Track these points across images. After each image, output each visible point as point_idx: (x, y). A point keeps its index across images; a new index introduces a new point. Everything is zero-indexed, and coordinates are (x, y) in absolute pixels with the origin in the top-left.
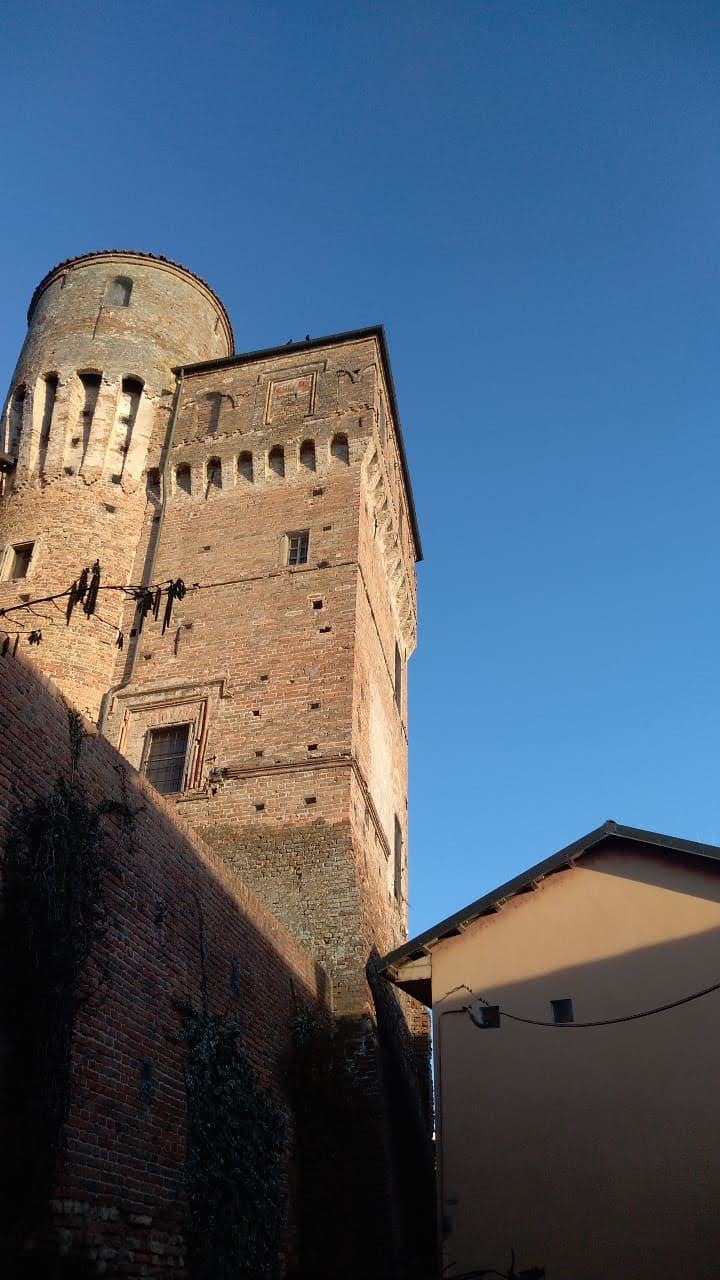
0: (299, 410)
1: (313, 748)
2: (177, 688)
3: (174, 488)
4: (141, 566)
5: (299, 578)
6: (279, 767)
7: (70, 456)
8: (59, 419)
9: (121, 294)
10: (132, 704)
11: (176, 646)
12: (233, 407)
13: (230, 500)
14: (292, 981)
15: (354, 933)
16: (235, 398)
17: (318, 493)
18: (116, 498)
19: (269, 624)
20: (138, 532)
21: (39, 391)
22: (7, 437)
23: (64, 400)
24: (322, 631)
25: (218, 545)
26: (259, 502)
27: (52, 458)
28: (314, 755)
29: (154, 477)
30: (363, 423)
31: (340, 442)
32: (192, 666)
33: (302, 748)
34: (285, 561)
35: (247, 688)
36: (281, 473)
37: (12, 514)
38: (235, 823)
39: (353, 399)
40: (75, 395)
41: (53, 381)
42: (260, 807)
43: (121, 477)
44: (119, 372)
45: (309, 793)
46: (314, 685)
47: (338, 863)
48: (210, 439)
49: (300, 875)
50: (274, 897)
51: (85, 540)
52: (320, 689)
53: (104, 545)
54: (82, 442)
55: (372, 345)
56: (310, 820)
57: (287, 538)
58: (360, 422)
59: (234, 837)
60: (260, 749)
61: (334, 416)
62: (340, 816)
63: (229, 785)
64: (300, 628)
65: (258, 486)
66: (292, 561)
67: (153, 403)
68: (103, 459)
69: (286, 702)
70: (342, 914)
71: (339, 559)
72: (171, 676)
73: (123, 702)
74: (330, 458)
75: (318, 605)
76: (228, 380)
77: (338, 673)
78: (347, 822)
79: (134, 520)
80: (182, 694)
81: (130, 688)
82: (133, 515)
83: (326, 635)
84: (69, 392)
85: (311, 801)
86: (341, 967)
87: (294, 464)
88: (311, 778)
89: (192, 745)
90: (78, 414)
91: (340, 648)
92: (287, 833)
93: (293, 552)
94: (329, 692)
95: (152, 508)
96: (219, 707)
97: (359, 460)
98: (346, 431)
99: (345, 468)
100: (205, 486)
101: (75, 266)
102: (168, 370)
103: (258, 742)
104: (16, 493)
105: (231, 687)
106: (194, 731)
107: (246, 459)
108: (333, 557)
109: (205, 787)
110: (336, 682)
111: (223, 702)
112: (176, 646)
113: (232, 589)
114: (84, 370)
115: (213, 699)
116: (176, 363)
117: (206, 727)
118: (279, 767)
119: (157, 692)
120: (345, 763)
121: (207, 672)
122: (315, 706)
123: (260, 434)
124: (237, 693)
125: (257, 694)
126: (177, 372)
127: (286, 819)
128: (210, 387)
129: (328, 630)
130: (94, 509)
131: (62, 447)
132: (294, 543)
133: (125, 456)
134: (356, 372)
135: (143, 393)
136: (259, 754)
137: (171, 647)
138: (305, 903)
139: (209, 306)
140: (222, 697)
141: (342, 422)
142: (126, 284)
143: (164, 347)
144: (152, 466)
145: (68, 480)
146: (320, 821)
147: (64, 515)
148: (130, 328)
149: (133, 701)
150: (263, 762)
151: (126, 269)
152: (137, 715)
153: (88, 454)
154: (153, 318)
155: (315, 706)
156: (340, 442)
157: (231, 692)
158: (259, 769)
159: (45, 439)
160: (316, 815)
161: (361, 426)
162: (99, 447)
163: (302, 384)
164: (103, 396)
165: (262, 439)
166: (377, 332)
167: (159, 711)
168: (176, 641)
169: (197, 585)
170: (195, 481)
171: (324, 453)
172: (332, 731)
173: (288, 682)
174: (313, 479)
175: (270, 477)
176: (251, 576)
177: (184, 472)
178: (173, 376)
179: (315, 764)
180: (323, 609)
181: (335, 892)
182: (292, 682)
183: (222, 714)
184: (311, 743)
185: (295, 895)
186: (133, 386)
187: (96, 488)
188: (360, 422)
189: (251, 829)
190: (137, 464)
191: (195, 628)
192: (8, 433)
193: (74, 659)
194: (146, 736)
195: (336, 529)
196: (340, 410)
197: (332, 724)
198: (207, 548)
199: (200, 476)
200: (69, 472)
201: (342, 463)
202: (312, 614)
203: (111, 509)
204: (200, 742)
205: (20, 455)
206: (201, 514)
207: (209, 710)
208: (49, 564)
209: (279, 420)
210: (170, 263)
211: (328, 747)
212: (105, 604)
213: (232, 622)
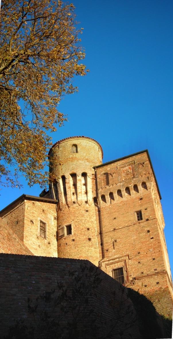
0: (130, 176)
2: (117, 258)
4: (98, 225)
6: (148, 276)
7: (74, 198)
9: (75, 149)
12: (112, 177)
13: (118, 203)
14: (112, 278)
16: (112, 174)
17: (141, 199)
20: (95, 215)
22: (54, 194)
24: (151, 239)
25: (118, 217)
26: (124, 204)
27: (69, 200)
28: (156, 272)
29: (95, 200)
30: (149, 178)
33: (153, 270)
34: (137, 220)
35: (135, 256)
37: (62, 216)
40: (70, 181)
41: (64, 178)
43: (87, 201)
45: (157, 281)
54: (76, 193)
55: (145, 154)
57: (136, 213)
58: (148, 178)
60: (142, 272)
61: (140, 177)
62: (166, 286)
65: (124, 199)
66: (139, 220)
68: (82, 198)
72: (115, 255)
74: (142, 189)
75: (148, 231)
76: (109, 169)
77: (158, 250)
79: (93, 212)
82: (93, 211)
84: (69, 180)
85: (158, 283)
87: (133, 192)
88: (157, 277)
89: (125, 272)
93: (138, 217)
94: (157, 254)
97: (150, 189)
99: (147, 191)
100: (110, 200)
101: (61, 143)
102: (92, 168)
103: (142, 270)
104: (61, 210)
106: (124, 269)
107: (119, 192)
108: (149, 217)
109: (131, 283)
115: (127, 260)
117: (127, 268)
121: (124, 253)
122: (154, 259)
124: (133, 258)
125: (138, 257)
126: (94, 168)
127: (153, 288)
128: (104, 171)
129: (152, 238)
130: (84, 212)
131: (71, 197)
132: (138, 214)
133: (87, 195)
135: (88, 176)
136: (142, 273)
137: (112, 247)
140: (129, 259)
141: (144, 179)
142: (75, 146)
143: (89, 162)
144: (94, 196)
146: (161, 288)
149: (107, 262)
152: (108, 266)
155: (154, 259)
156: (144, 185)
158: (143, 277)
161: (148, 179)
162: (80, 194)
164: (78, 180)
166: (146, 151)
167: (114, 264)
168: (113, 245)
173: (146, 253)
175: (127, 196)
176: (129, 225)
177: (103, 197)
178: (93, 169)
179: (157, 274)
180: (150, 233)
182: (147, 253)
184: (155, 269)
186: (84, 175)
188: (148, 178)
190: (91, 196)
192: (54, 193)
193: (90, 254)
194: (112, 271)
195: (148, 209)
196: (142, 175)
198: (115, 218)
201: (146, 190)
203: (87, 211)
204: (126, 271)
205: (60, 199)
206: (111, 208)
207: (127, 263)
211: (159, 269)
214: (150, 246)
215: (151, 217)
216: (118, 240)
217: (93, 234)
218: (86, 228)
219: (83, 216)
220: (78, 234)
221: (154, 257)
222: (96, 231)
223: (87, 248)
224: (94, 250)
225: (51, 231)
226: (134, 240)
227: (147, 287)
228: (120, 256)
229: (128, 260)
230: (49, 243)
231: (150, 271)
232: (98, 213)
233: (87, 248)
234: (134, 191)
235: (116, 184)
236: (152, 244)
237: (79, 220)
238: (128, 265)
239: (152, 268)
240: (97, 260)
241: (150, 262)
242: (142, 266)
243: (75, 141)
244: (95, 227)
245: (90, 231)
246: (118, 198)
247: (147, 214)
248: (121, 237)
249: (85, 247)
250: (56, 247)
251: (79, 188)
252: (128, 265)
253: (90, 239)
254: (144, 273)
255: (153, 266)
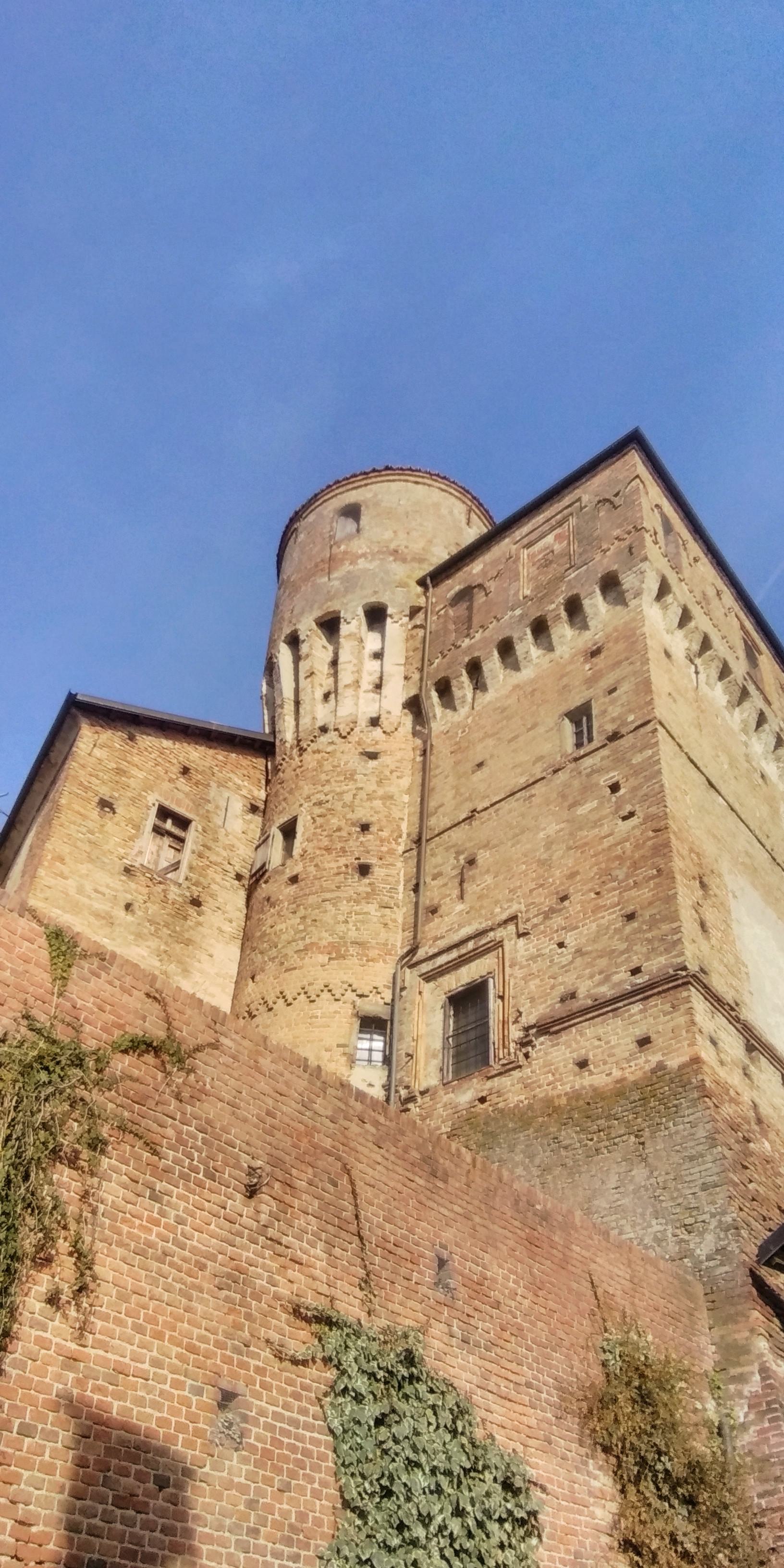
1: (636, 971)
3: (438, 710)
5: (588, 762)
7: (322, 713)
8: (306, 677)
10: (424, 971)
11: (462, 891)
15: (724, 1213)
17: (595, 653)
18: (377, 743)
19: (560, 831)
21: (284, 656)
23: (307, 656)
24: (625, 818)
25: (492, 756)
26: (530, 693)
27: (305, 721)
31: (610, 585)
32: (481, 907)
36: (550, 648)
38: (555, 1093)
39: (620, 526)
40: (317, 648)
41: (294, 641)
42: (583, 1064)
44: (357, 606)
45: (639, 1031)
46: (625, 891)
47: (691, 1118)
48: (467, 641)
49: (643, 1144)
50: (613, 1181)
51: (348, 798)
52: (633, 893)
53: (370, 797)
55: (634, 460)
56: (647, 1068)
57: (567, 721)
59: (556, 1109)
63: (542, 1044)
64: (597, 823)
65: (527, 673)
66: (579, 745)
67: (402, 625)
69: (594, 921)
70: (705, 1187)
71: (632, 722)
72: (461, 926)
73: (416, 971)
75: (615, 788)
78: (696, 1060)
80: (481, 944)
81: (421, 953)
82: (399, 755)
83: (634, 821)
85: (644, 1042)
86: (711, 1264)
88: (641, 1011)
89: (493, 1004)
90: (326, 667)
91: (651, 834)
92: (621, 1091)
93: (579, 734)
94: (646, 893)
95: (419, 742)
96: (518, 949)
98: (615, 567)
100: (469, 696)
102: (413, 584)
103: (567, 981)
105: (528, 920)
108: (624, 723)
110: (653, 878)
111: (522, 941)
112: (462, 891)
113: (512, 803)
114: (322, 617)
115: (510, 940)
116: (420, 574)
117: (507, 978)
118: (601, 1007)
119: (449, 949)
120: (680, 982)
121: (498, 910)
122: (630, 917)
123: (518, 612)
125: (557, 921)
126: (422, 583)
127: (617, 1074)
129: (631, 814)
134: (616, 495)
137: (456, 892)
138: (653, 1181)
139: (453, 500)
141: (603, 563)
145: (324, 739)
146: (661, 1066)
147: (323, 777)
148: (364, 555)
149: (425, 967)
150: (575, 1005)
151: (351, 497)
153: (340, 704)
154: (388, 535)
155: (630, 917)
156: (610, 585)
157: (528, 926)
159: (297, 703)
160: (655, 1059)
161: (631, 554)
162: (350, 692)
163: (557, 537)
165: (522, 616)
166: (634, 440)
168: (462, 882)
169: (475, 810)
170: (457, 693)
171: (596, 605)
172: (656, 944)
173: (593, 895)
174: (587, 639)
175: (538, 657)
178: (419, 589)
180: (622, 791)
181: (691, 1158)
182: (598, 893)
183: (523, 956)
184: (633, 965)
185: (639, 1173)
187: (353, 738)
189: (575, 1096)
190: (396, 694)
191: (480, 860)
193: (353, 934)
196: (605, 547)
197: (655, 932)
198: (480, 765)
199: (463, 687)
200: (324, 730)
202: (609, 800)
203: (373, 756)
208: (314, 834)
209: (537, 588)
210: (398, 469)
211: (656, 965)
212: (380, 862)
213: (518, 842)
214: (618, 857)
215: (631, 718)
216: (483, 857)
217: (384, 849)
218: (353, 825)
219: (351, 776)
220: (318, 852)
221: (630, 909)
222: (405, 836)
223: (344, 906)
224: (379, 914)
225: (218, 854)
226: (549, 844)
227: (592, 1067)
228: (484, 925)
229: (513, 942)
230: (196, 903)
231: (607, 979)
232: (419, 759)
233: (344, 906)
234: (567, 627)
235: (498, 620)
236: (628, 844)
237: (329, 797)
238: (510, 966)
239: (617, 965)
240: (385, 961)
241: (611, 932)
242: (572, 962)
243: (354, 492)
244: (403, 819)
245: (370, 837)
246: (501, 677)
247: (615, 711)
248: (495, 842)
249: (335, 902)
250: (234, 924)
251: (345, 670)
252: (510, 966)
253: (364, 870)
254: (582, 993)
255: (622, 953)
